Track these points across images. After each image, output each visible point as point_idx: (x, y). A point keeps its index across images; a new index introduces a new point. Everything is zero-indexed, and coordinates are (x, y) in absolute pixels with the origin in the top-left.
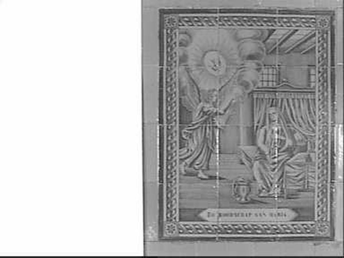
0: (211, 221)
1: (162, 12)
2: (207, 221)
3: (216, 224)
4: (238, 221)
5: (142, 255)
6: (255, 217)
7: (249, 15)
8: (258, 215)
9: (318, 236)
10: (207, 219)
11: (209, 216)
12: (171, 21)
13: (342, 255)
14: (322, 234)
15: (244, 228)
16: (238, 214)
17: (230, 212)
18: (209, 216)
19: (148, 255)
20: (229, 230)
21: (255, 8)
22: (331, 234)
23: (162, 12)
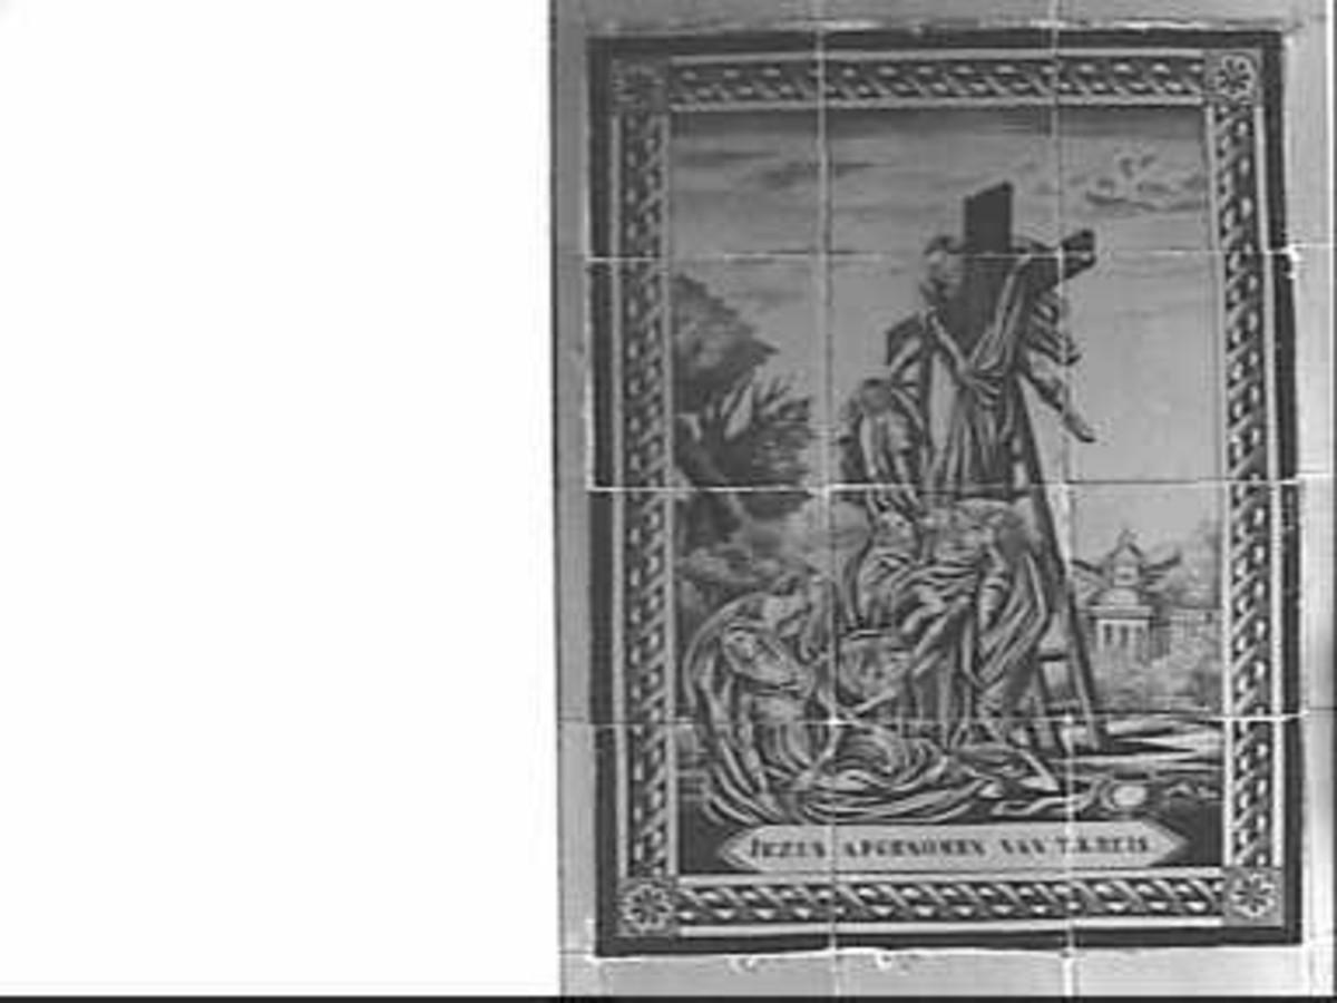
0: (770, 871)
1: (1268, 42)
2: (754, 872)
3: (826, 880)
4: (1088, 865)
5: (553, 990)
6: (848, 859)
7: (940, 55)
8: (1032, 848)
9: (1237, 922)
10: (753, 863)
11: (754, 854)
12: (640, 86)
13: (1329, 992)
14: (1252, 915)
15: (862, 897)
16: (1117, 841)
17: (891, 838)
18: (754, 854)
19: (570, 992)
20: (1196, 900)
21: (709, 31)
22: (1287, 917)
23: (1268, 42)
